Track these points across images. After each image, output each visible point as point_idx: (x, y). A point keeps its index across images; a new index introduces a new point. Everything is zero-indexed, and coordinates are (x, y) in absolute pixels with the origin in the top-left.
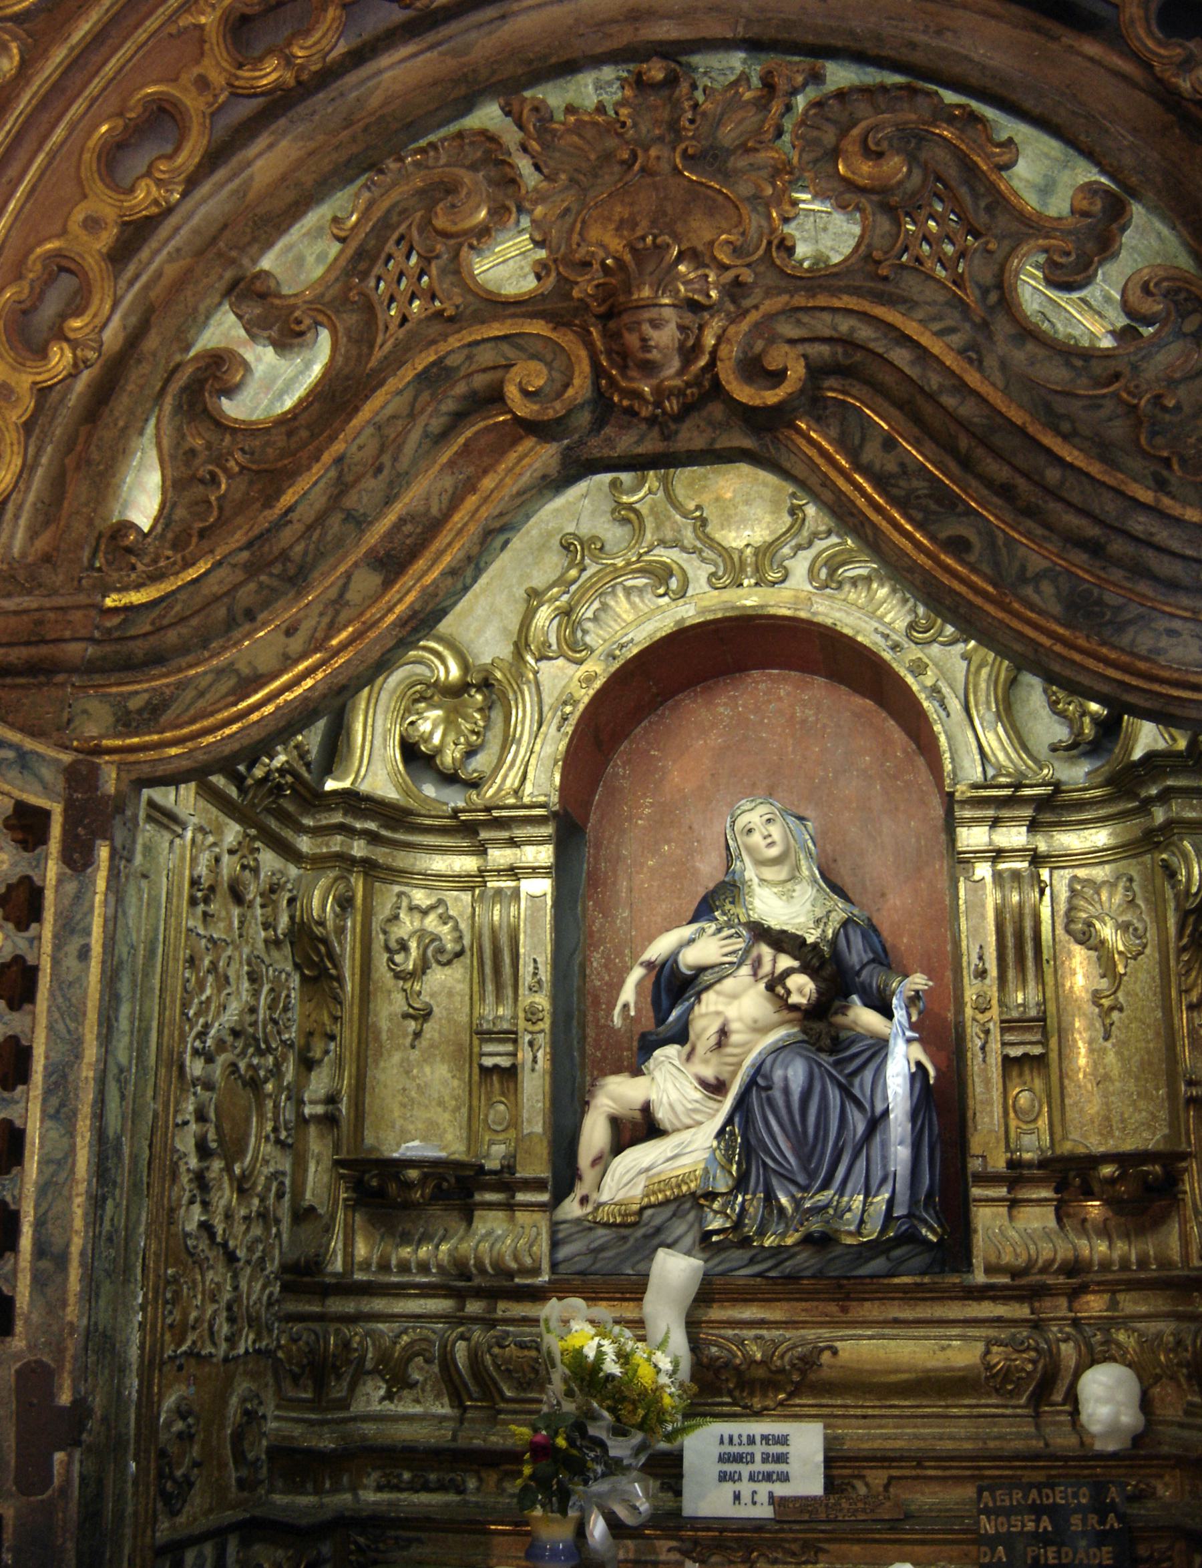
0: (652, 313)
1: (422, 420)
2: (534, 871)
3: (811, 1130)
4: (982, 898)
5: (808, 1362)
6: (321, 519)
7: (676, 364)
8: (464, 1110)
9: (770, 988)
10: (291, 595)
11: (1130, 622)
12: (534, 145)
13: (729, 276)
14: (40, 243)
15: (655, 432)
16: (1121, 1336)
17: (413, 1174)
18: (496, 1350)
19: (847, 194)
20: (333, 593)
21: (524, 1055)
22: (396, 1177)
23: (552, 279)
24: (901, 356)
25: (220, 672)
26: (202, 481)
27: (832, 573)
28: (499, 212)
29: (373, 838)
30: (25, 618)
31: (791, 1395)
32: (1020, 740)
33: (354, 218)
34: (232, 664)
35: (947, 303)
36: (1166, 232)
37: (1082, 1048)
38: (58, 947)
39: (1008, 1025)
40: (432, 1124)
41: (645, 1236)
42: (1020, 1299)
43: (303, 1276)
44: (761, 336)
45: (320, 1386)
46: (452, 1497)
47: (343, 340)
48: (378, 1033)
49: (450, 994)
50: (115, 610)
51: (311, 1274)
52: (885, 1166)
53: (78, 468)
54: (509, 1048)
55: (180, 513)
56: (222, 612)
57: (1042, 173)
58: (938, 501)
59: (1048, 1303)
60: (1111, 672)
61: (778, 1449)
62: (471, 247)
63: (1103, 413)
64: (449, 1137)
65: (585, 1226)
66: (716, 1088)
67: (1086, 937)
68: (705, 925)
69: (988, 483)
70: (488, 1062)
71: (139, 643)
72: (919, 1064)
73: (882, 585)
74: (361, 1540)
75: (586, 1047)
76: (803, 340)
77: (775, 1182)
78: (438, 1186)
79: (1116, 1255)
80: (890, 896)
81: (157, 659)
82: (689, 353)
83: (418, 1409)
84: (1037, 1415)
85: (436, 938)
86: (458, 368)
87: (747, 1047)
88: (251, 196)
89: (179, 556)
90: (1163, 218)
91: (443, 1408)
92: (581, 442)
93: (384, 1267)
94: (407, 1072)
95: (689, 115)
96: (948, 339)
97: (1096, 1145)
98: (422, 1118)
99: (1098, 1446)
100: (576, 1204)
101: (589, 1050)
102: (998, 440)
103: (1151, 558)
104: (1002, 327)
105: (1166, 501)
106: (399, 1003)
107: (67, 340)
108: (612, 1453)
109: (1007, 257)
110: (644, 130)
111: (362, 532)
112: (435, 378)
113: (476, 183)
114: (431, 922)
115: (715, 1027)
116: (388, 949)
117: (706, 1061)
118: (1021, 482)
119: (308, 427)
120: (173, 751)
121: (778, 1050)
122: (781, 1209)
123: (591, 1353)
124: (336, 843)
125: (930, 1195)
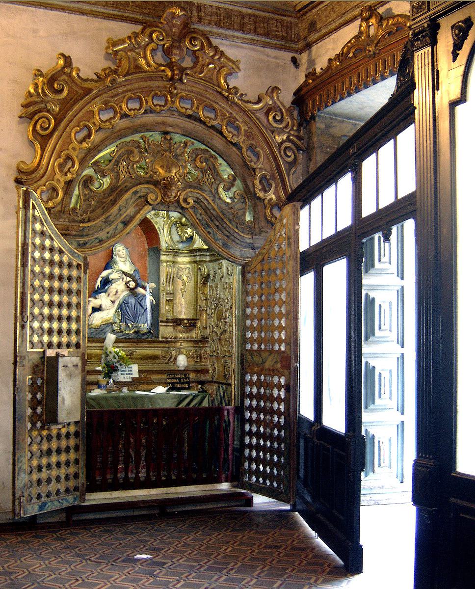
6: (117, 214)
9: (126, 284)
24: (206, 202)
25: (96, 238)
57: (226, 172)
61: (130, 369)
66: (113, 302)
69: (215, 225)
87: (120, 294)
99: (180, 369)
112: (136, 193)
118: (220, 226)
122: (129, 326)
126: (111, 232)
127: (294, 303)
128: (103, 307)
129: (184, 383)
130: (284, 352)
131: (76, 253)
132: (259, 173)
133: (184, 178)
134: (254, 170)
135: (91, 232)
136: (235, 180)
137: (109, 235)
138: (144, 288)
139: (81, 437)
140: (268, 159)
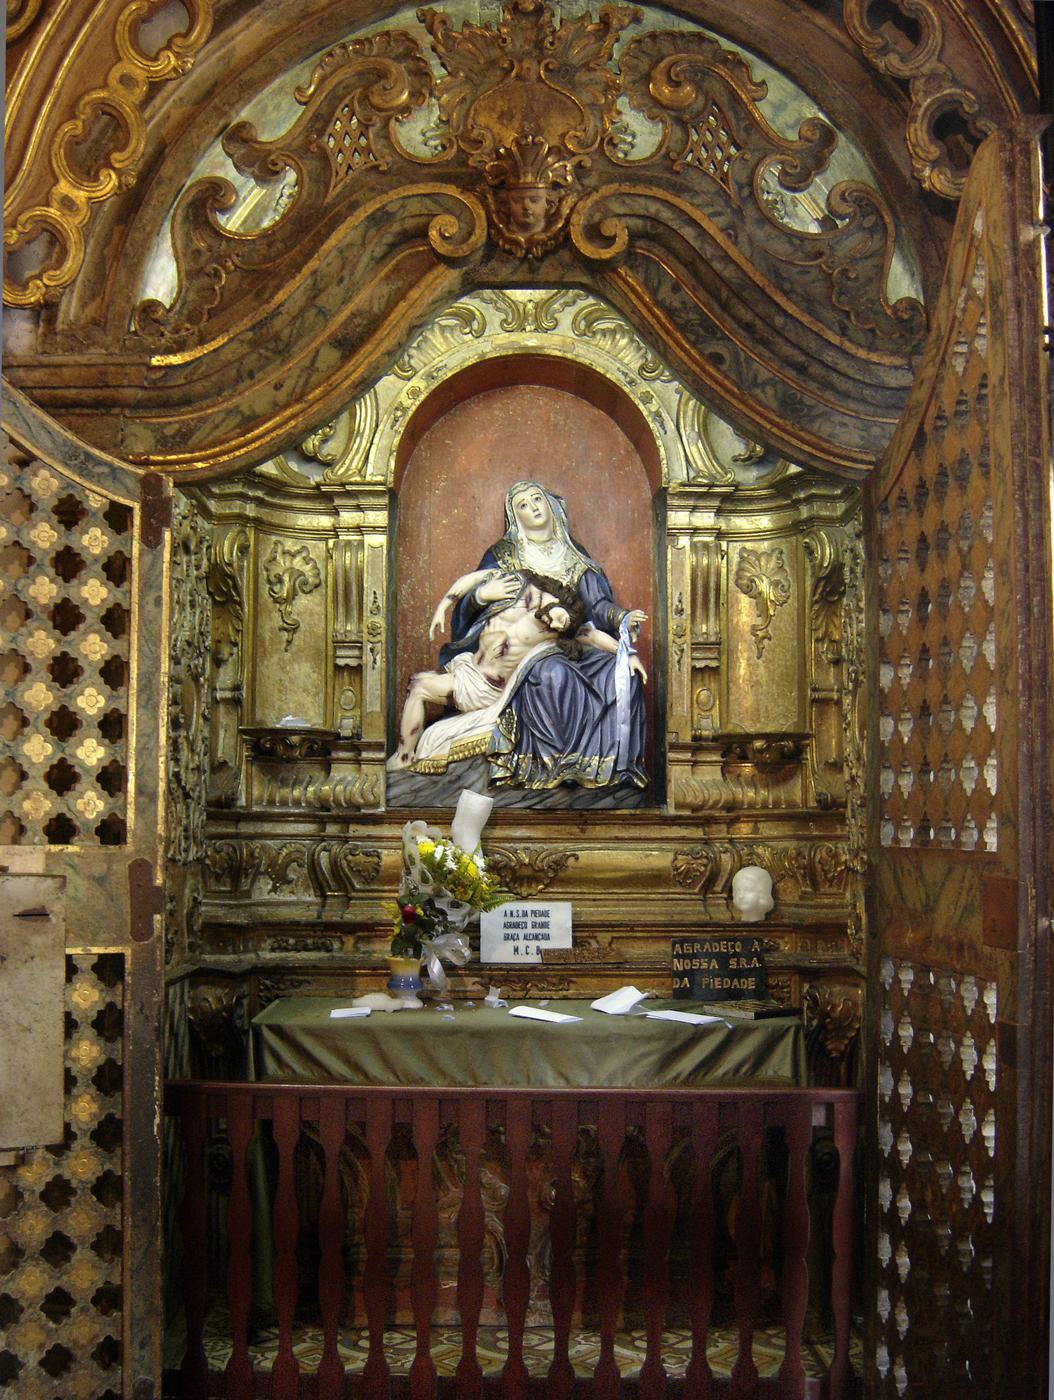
0: (532, 193)
1: (370, 248)
2: (374, 529)
3: (566, 713)
4: (682, 559)
5: (559, 865)
6: (302, 312)
7: (542, 224)
8: (322, 695)
9: (538, 616)
10: (278, 362)
11: (818, 416)
12: (441, 49)
13: (576, 160)
14: (88, 91)
15: (525, 266)
16: (760, 850)
17: (295, 739)
18: (350, 857)
19: (654, 108)
20: (307, 362)
21: (368, 658)
22: (283, 741)
23: (452, 152)
24: (688, 233)
25: (229, 412)
26: (208, 275)
27: (589, 325)
28: (416, 95)
29: (260, 502)
30: (93, 370)
31: (547, 886)
32: (712, 452)
33: (312, 89)
34: (237, 407)
35: (716, 193)
36: (857, 155)
37: (743, 663)
38: (141, 598)
39: (696, 646)
40: (301, 705)
41: (451, 782)
42: (697, 825)
43: (222, 809)
44: (598, 210)
45: (236, 882)
46: (323, 954)
47: (306, 179)
48: (263, 641)
49: (311, 614)
50: (159, 368)
51: (229, 807)
52: (613, 738)
53: (116, 258)
54: (356, 653)
55: (192, 296)
56: (233, 373)
57: (783, 107)
58: (706, 329)
59: (715, 828)
60: (806, 448)
62: (397, 120)
63: (809, 278)
64: (311, 713)
65: (408, 775)
66: (498, 683)
67: (749, 589)
68: (494, 571)
69: (738, 321)
70: (341, 662)
71: (176, 390)
72: (637, 671)
73: (623, 337)
74: (268, 982)
75: (410, 656)
76: (625, 215)
77: (539, 746)
78: (311, 748)
79: (759, 799)
80: (612, 552)
81: (186, 402)
82: (551, 218)
83: (293, 898)
84: (705, 900)
85: (301, 574)
86: (395, 213)
87: (521, 655)
88: (233, 64)
89: (196, 329)
90: (857, 147)
91: (310, 897)
92: (474, 270)
93: (271, 802)
94: (283, 668)
95: (550, 39)
96: (716, 219)
97: (750, 728)
98: (296, 704)
99: (745, 918)
100: (399, 759)
101: (400, 653)
102: (746, 294)
103: (836, 379)
104: (750, 213)
105: (847, 345)
106: (276, 621)
107: (114, 169)
108: (450, 919)
109: (757, 165)
110: (518, 44)
111: (327, 321)
112: (380, 219)
113: (400, 73)
114: (298, 563)
115: (499, 642)
116: (269, 581)
117: (492, 665)
118: (758, 323)
119: (283, 241)
120: (200, 465)
121: (544, 658)
122: (544, 765)
123: (438, 856)
124: (236, 507)
125: (639, 757)
126: (289, 384)
127: (1028, 609)
128: (461, 700)
129: (739, 974)
130: (992, 860)
131: (100, 462)
132: (927, 94)
133: (601, 149)
134: (904, 84)
135: (198, 387)
136: (828, 139)
137: (281, 396)
138: (613, 632)
139: (128, 1199)
140: (965, 35)
